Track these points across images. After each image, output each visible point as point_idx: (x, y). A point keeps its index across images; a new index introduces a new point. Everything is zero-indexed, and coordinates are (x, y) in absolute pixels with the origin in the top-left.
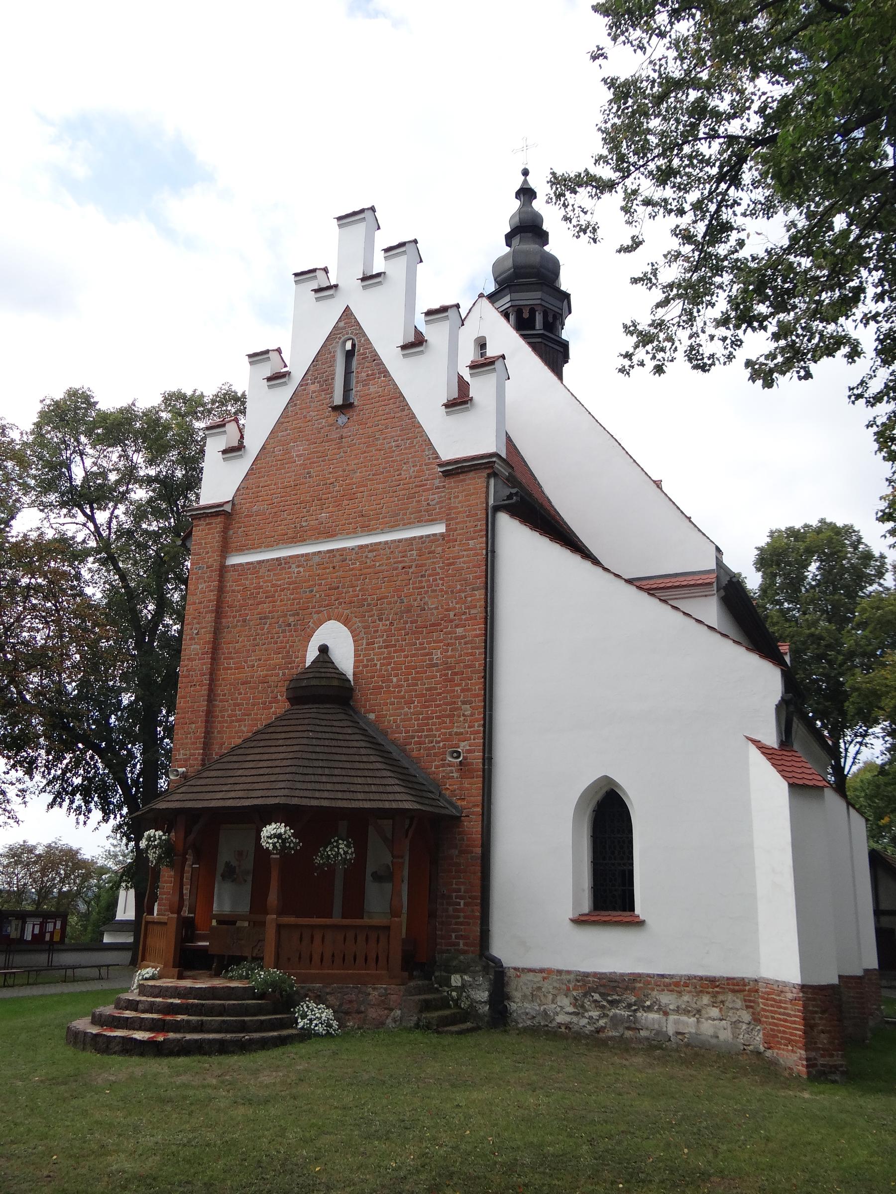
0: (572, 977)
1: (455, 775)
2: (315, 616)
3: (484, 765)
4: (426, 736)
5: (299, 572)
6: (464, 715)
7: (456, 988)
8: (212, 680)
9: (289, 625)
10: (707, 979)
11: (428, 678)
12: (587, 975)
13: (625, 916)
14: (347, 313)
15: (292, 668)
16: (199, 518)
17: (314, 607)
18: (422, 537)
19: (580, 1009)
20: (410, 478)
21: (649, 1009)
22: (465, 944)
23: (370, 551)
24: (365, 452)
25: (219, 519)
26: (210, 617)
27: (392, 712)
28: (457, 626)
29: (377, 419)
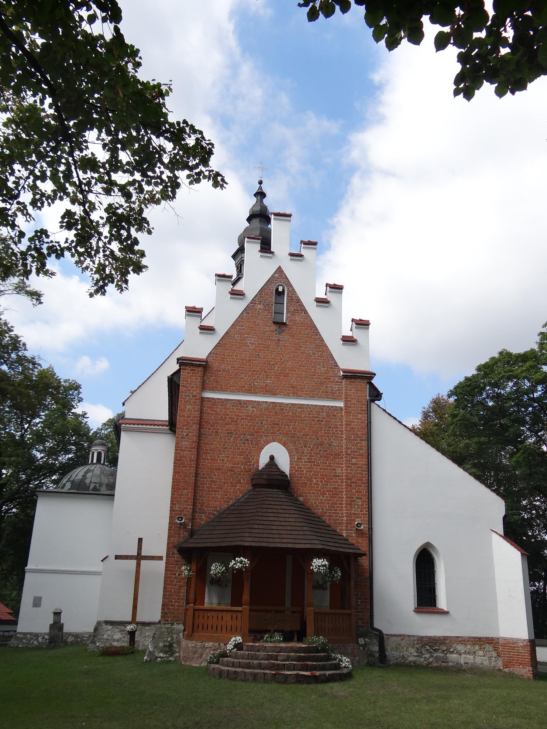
0: (415, 638)
1: (354, 535)
2: (265, 438)
3: (369, 531)
4: (334, 513)
5: (253, 411)
6: (358, 505)
7: (362, 645)
8: (197, 464)
9: (248, 440)
10: (477, 638)
11: (334, 482)
12: (422, 637)
13: (431, 609)
14: (280, 270)
15: (250, 465)
16: (186, 366)
17: (263, 433)
18: (329, 406)
19: (420, 654)
20: (321, 373)
21: (452, 652)
22: (362, 623)
23: (298, 408)
24: (294, 352)
25: (200, 369)
26: (196, 427)
27: (314, 498)
28: (353, 458)
29: (300, 335)
